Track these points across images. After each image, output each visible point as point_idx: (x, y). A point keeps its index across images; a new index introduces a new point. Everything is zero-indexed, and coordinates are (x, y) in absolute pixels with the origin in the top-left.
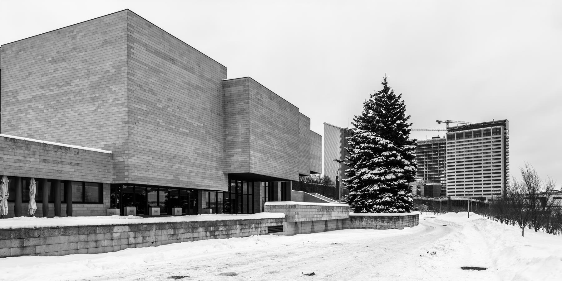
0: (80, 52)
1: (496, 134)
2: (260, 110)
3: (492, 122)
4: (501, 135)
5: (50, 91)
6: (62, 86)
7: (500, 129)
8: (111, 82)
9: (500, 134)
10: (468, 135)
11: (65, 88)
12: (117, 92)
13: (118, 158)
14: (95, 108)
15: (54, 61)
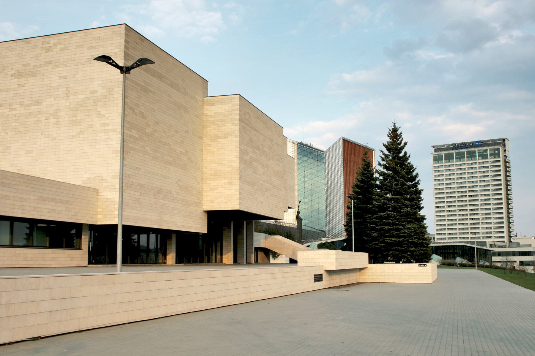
0: (57, 66)
1: (495, 158)
2: (249, 132)
3: (488, 141)
4: (501, 159)
5: (11, 110)
6: (29, 105)
7: (498, 149)
8: (99, 104)
9: (499, 157)
10: (460, 157)
11: (33, 107)
12: (106, 115)
13: (105, 194)
14: (75, 134)
15: (19, 75)
